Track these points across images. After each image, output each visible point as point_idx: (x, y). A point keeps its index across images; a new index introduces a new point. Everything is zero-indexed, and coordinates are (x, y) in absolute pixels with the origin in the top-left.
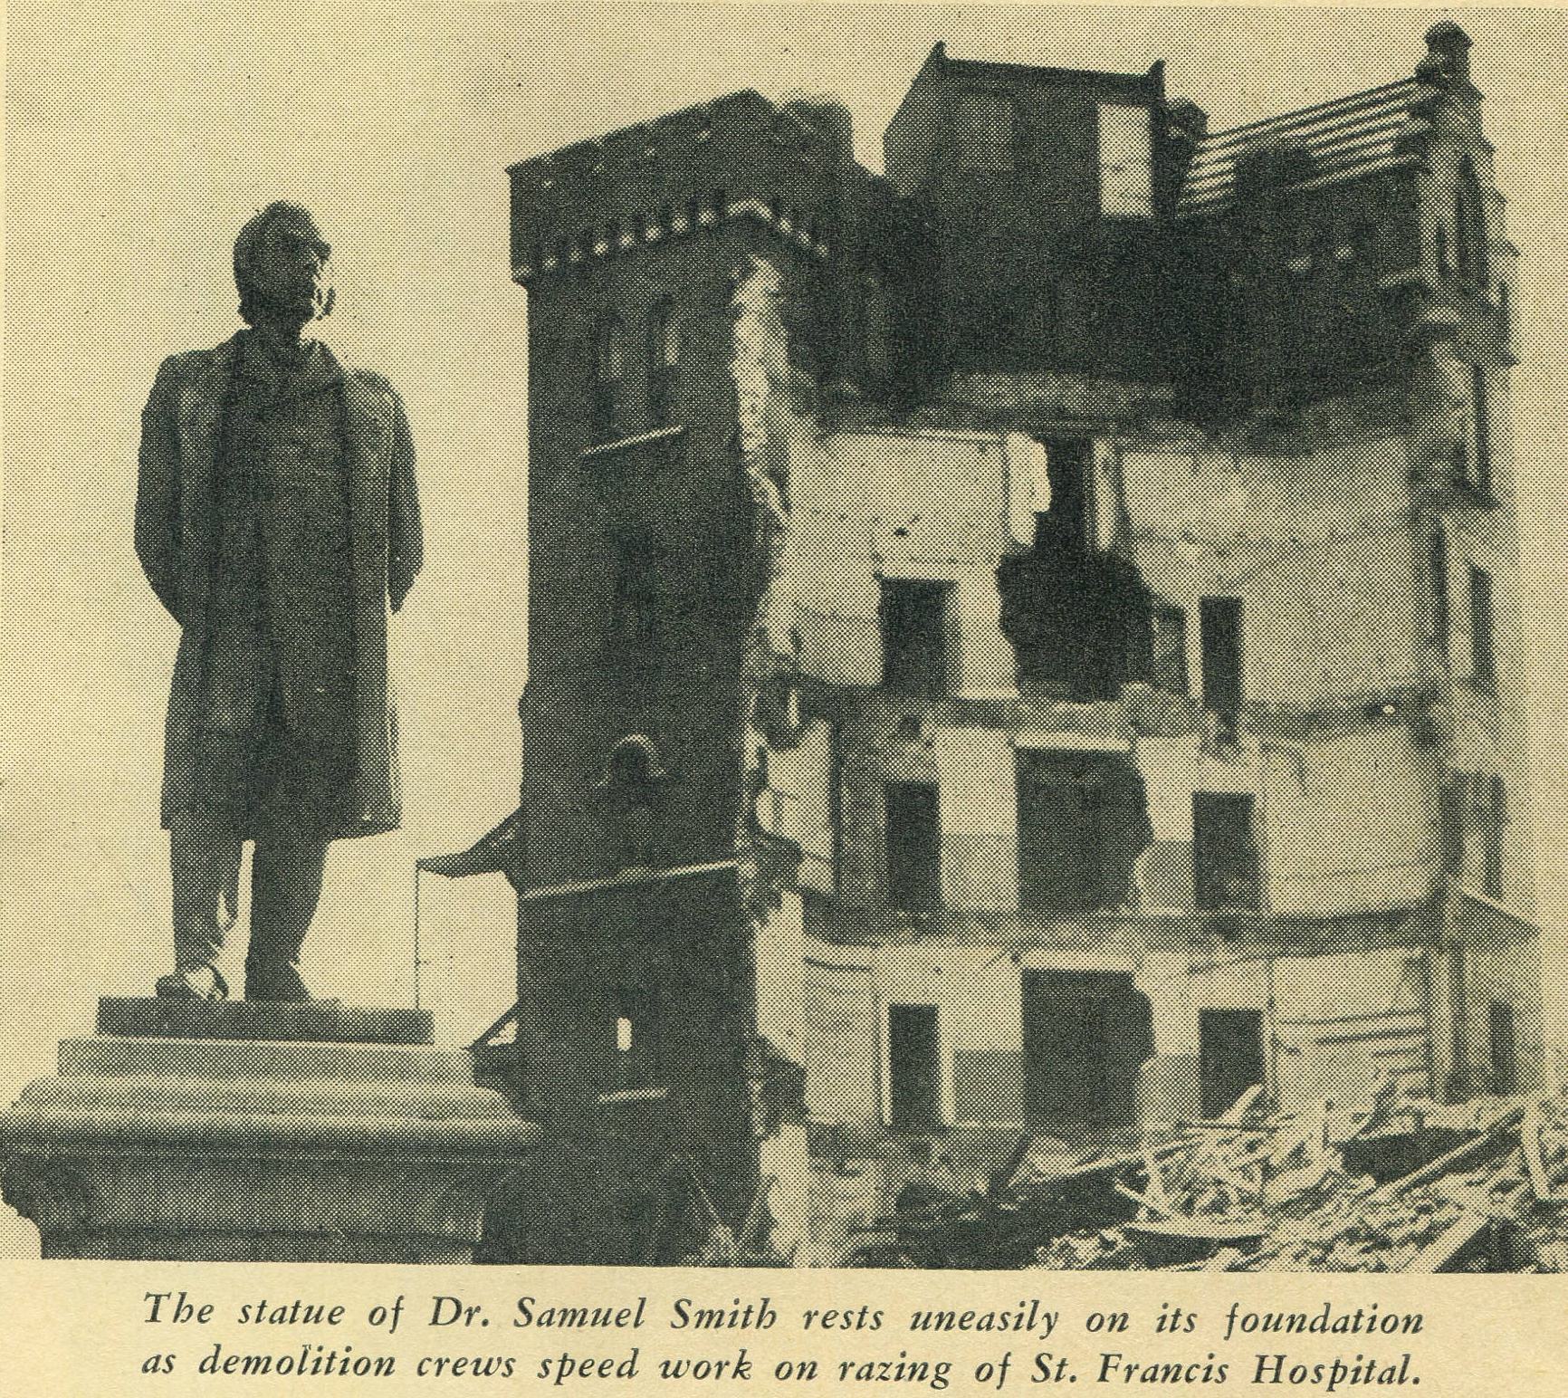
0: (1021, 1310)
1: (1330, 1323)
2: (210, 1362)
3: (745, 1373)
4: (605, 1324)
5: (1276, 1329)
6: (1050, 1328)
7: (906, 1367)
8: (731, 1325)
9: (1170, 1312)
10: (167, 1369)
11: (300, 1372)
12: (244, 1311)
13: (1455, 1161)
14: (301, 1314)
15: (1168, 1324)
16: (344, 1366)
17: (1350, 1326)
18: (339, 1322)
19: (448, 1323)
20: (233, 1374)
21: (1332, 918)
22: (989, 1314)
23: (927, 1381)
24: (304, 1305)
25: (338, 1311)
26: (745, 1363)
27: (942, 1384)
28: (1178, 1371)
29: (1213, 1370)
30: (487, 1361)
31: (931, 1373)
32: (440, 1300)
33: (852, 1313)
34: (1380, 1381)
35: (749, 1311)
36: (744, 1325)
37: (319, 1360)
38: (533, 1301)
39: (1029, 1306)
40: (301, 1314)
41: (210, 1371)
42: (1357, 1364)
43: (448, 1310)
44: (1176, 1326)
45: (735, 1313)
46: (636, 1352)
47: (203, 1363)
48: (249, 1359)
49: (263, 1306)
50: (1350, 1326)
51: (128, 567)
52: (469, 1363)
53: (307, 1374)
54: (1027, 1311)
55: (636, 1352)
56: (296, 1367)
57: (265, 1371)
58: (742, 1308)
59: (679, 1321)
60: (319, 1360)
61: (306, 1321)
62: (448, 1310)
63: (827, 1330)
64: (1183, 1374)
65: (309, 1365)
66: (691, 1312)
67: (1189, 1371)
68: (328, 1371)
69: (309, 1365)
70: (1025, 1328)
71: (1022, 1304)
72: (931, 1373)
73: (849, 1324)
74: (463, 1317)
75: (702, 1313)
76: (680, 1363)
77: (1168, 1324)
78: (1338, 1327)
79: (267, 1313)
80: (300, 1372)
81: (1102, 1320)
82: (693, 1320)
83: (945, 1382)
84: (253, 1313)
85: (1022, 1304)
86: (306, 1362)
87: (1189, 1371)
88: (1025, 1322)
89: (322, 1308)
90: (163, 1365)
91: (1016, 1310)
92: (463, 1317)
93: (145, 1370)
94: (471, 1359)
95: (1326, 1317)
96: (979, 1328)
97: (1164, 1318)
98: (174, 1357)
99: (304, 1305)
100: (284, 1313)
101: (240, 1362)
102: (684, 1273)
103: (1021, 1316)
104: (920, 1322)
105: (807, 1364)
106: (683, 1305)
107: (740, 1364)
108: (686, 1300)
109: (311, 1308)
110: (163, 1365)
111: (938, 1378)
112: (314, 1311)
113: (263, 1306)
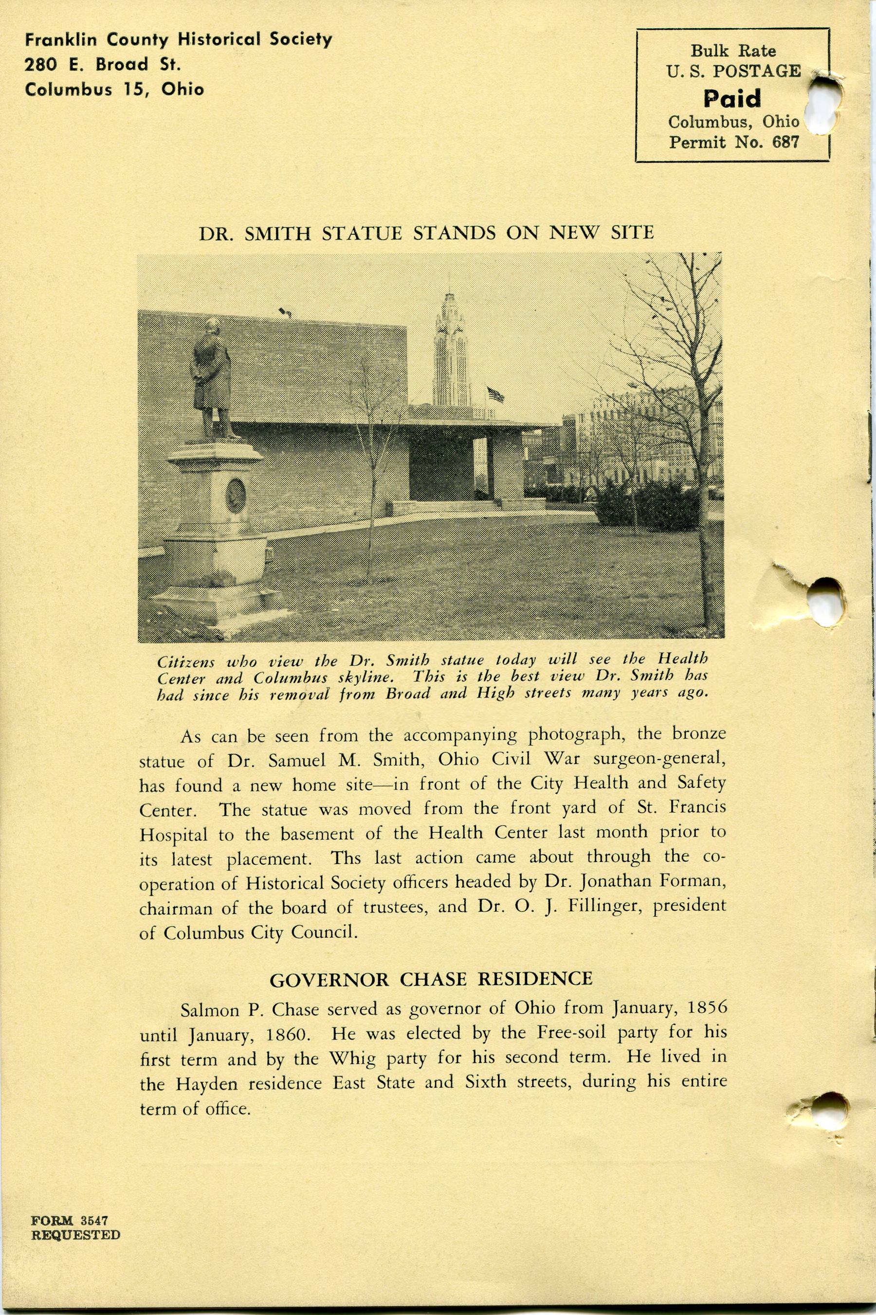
0: (564, 656)
1: (520, 661)
6: (533, 663)
8: (411, 664)
10: (464, 680)
13: (259, 627)
14: (466, 661)
15: (173, 664)
17: (461, 662)
23: (685, 697)
24: (468, 657)
27: (501, 699)
28: (212, 696)
31: (686, 693)
32: (354, 656)
35: (418, 659)
36: (175, 666)
40: (466, 661)
43: (357, 660)
45: (413, 659)
47: (672, 677)
48: (292, 677)
49: (451, 658)
50: (461, 662)
54: (567, 656)
56: (273, 680)
57: (299, 682)
58: (415, 657)
59: (390, 663)
61: (468, 663)
63: (332, 667)
64: (214, 697)
65: (367, 678)
66: (395, 659)
67: (217, 695)
68: (661, 679)
69: (367, 678)
72: (686, 693)
73: (445, 663)
74: (364, 662)
75: (399, 660)
77: (173, 664)
80: (275, 682)
81: (250, 664)
82: (395, 662)
83: (503, 698)
84: (447, 661)
85: (565, 654)
87: (217, 695)
88: (566, 661)
90: (702, 677)
91: (562, 656)
92: (364, 662)
93: (217, 683)
94: (573, 674)
96: (681, 662)
97: (171, 662)
99: (468, 657)
103: (564, 658)
106: (392, 657)
110: (702, 677)
111: (499, 697)
113: (451, 658)
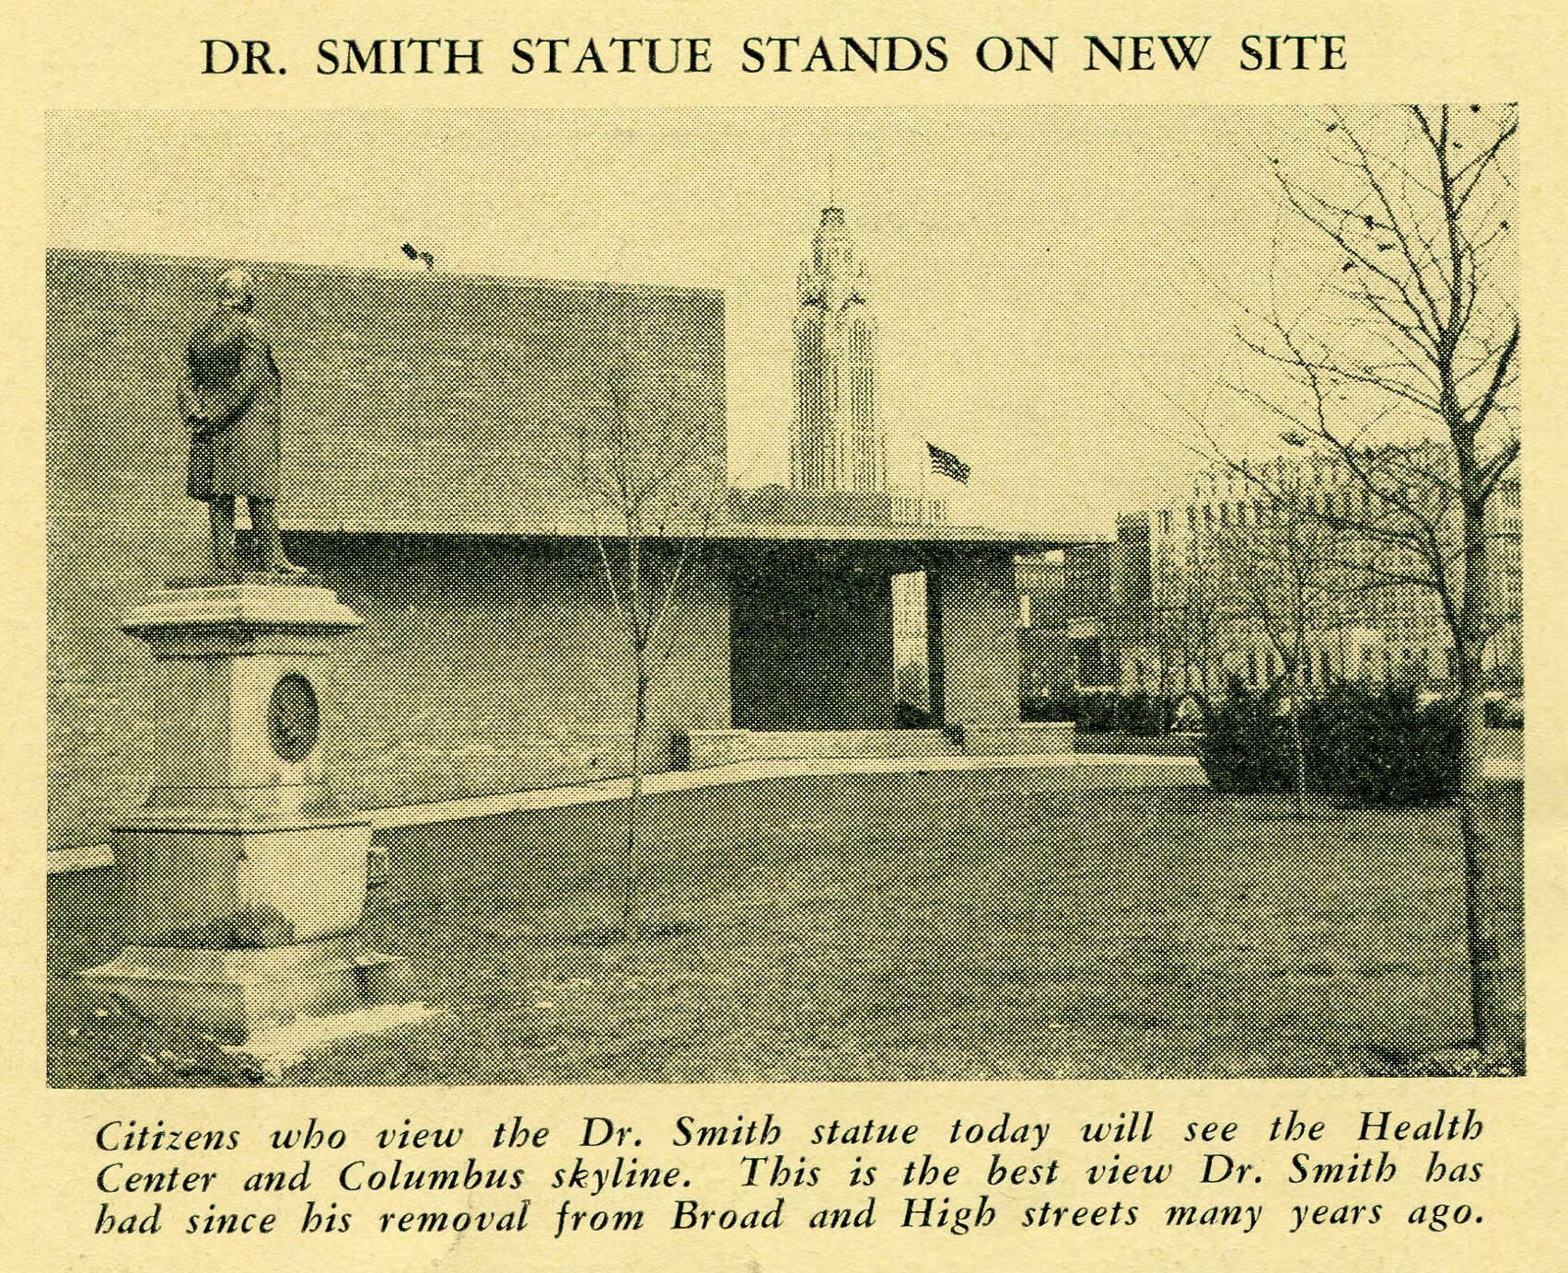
0: (1122, 1121)
1: (1008, 1133)
2: (300, 1178)
3: (582, 1181)
4: (891, 1140)
5: (891, 1140)
6: (1041, 1139)
7: (638, 1173)
9: (137, 1130)
11: (393, 1186)
12: (817, 1132)
14: (875, 1133)
15: (135, 1141)
16: (799, 1177)
17: (860, 1136)
18: (1319, 1137)
19: (599, 1144)
20: (953, 1185)
21: (1470, 930)
22: (1426, 1123)
25: (543, 1133)
26: (582, 1172)
29: (1467, 1168)
30: (1158, 1169)
32: (591, 1121)
33: (823, 1127)
34: (291, 1188)
35: (752, 1128)
36: (141, 1146)
37: (633, 1173)
38: (692, 1120)
39: (1130, 1118)
40: (875, 1133)
41: (299, 1188)
42: (1353, 1162)
43: (599, 1131)
44: (752, 1139)
46: (308, 1164)
49: (834, 1127)
50: (860, 1136)
51: (512, 801)
52: (1140, 1170)
53: (621, 1187)
54: (1128, 1122)
55: (308, 1164)
57: (452, 1186)
58: (746, 1125)
59: (681, 1138)
60: (633, 1173)
61: (880, 1140)
62: (599, 1131)
68: (1364, 1179)
69: (624, 1177)
70: (1432, 1138)
71: (1123, 1116)
75: (704, 1131)
76: (1162, 1168)
77: (135, 1141)
78: (848, 1138)
79: (839, 1134)
80: (393, 1186)
84: (825, 1134)
85: (1123, 1116)
86: (398, 1177)
88: (1125, 1133)
89: (895, 1128)
90: (1470, 1173)
92: (616, 1137)
93: (247, 1188)
94: (1142, 1167)
95: (1004, 1126)
96: (1416, 1137)
97: (131, 1136)
98: (874, 1169)
100: (856, 1134)
101: (142, 1180)
102: (139, 1096)
103: (1121, 1127)
104: (281, 1141)
105: (275, 1175)
106: (686, 1123)
107: (577, 1172)
108: (690, 1118)
109: (884, 1128)
110: (1470, 1173)
112: (442, 1135)
113: (834, 1127)
